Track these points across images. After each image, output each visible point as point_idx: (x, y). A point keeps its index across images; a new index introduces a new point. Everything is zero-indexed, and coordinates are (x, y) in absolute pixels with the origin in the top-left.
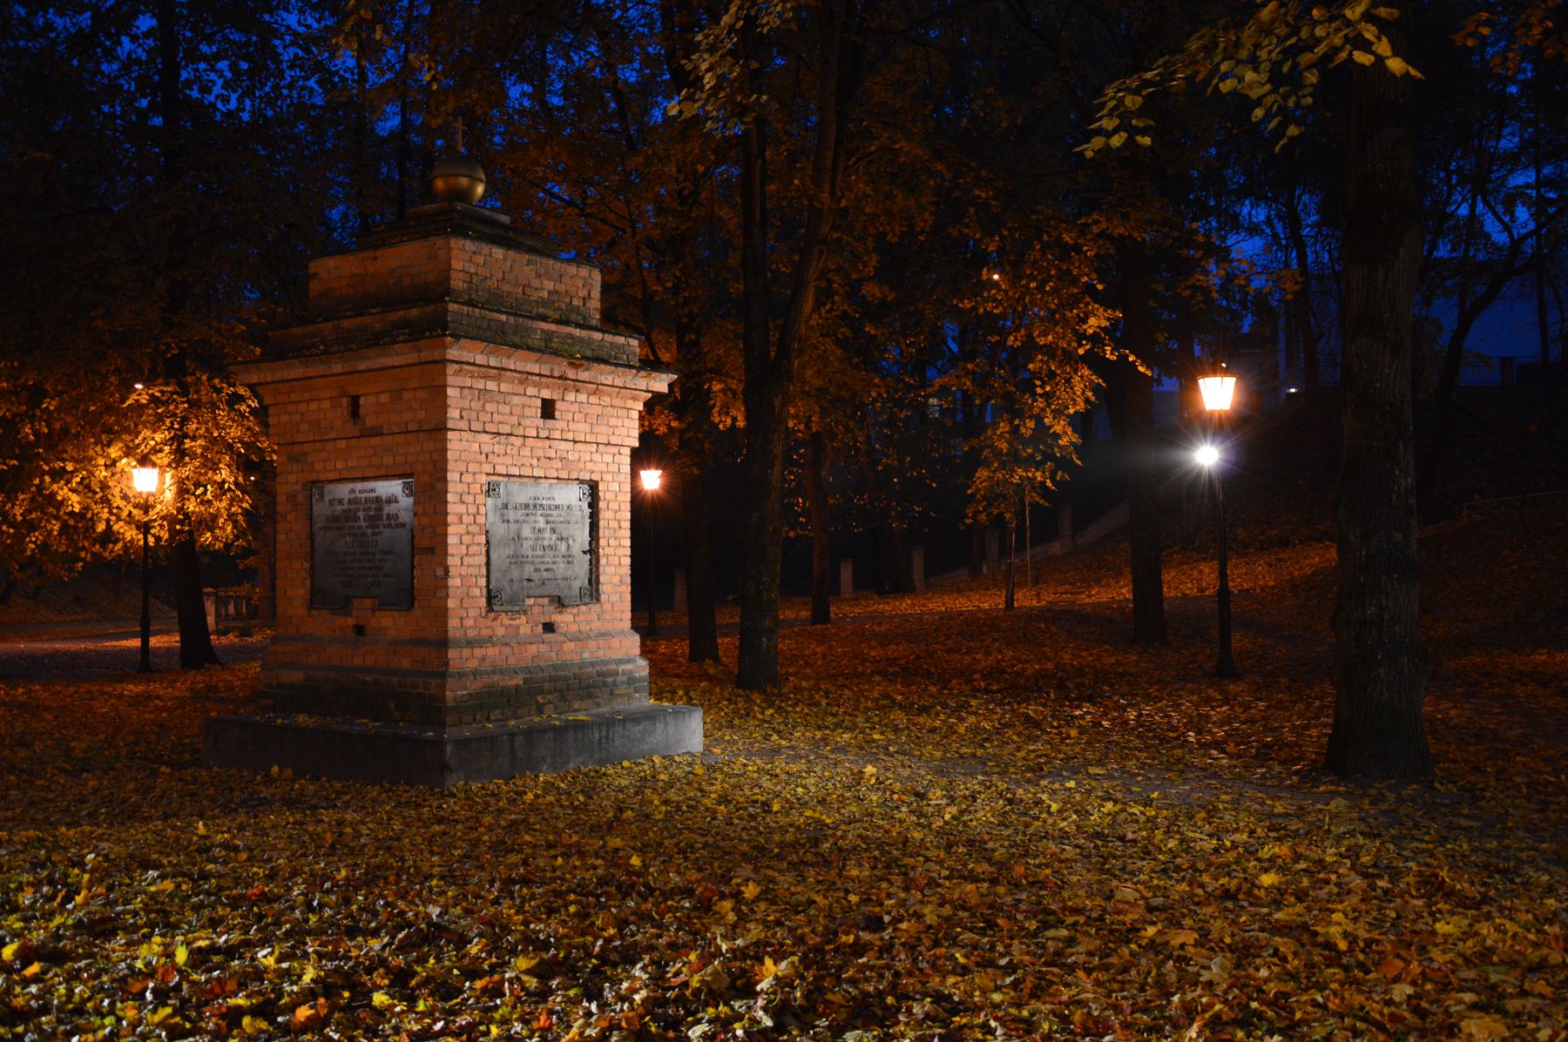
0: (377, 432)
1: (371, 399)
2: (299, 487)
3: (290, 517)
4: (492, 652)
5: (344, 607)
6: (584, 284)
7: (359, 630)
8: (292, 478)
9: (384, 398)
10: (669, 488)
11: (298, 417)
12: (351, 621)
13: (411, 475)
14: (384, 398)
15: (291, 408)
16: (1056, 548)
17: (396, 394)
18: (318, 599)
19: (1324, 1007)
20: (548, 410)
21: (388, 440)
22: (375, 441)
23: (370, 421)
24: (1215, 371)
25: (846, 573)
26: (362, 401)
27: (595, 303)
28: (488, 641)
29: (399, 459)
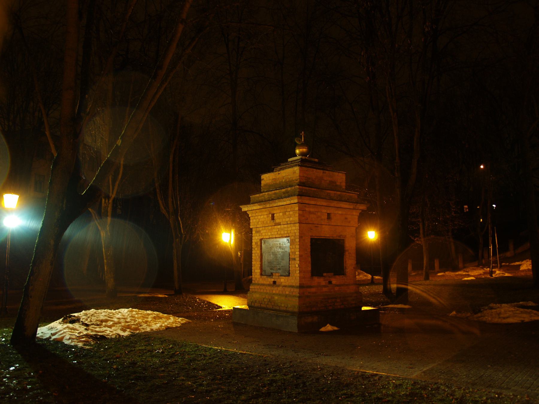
0: (279, 224)
1: (278, 215)
2: (258, 240)
3: (256, 249)
4: (313, 290)
5: (271, 275)
6: (340, 178)
7: (274, 282)
8: (256, 238)
9: (281, 214)
10: (384, 238)
11: (258, 220)
12: (273, 280)
13: (289, 237)
14: (281, 214)
15: (256, 217)
16: (508, 254)
17: (284, 213)
18: (262, 273)
19: (229, 392)
20: (329, 216)
21: (282, 226)
22: (279, 227)
23: (277, 221)
24: (237, 239)
25: (437, 264)
26: (275, 215)
27: (344, 184)
28: (310, 287)
29: (286, 232)
